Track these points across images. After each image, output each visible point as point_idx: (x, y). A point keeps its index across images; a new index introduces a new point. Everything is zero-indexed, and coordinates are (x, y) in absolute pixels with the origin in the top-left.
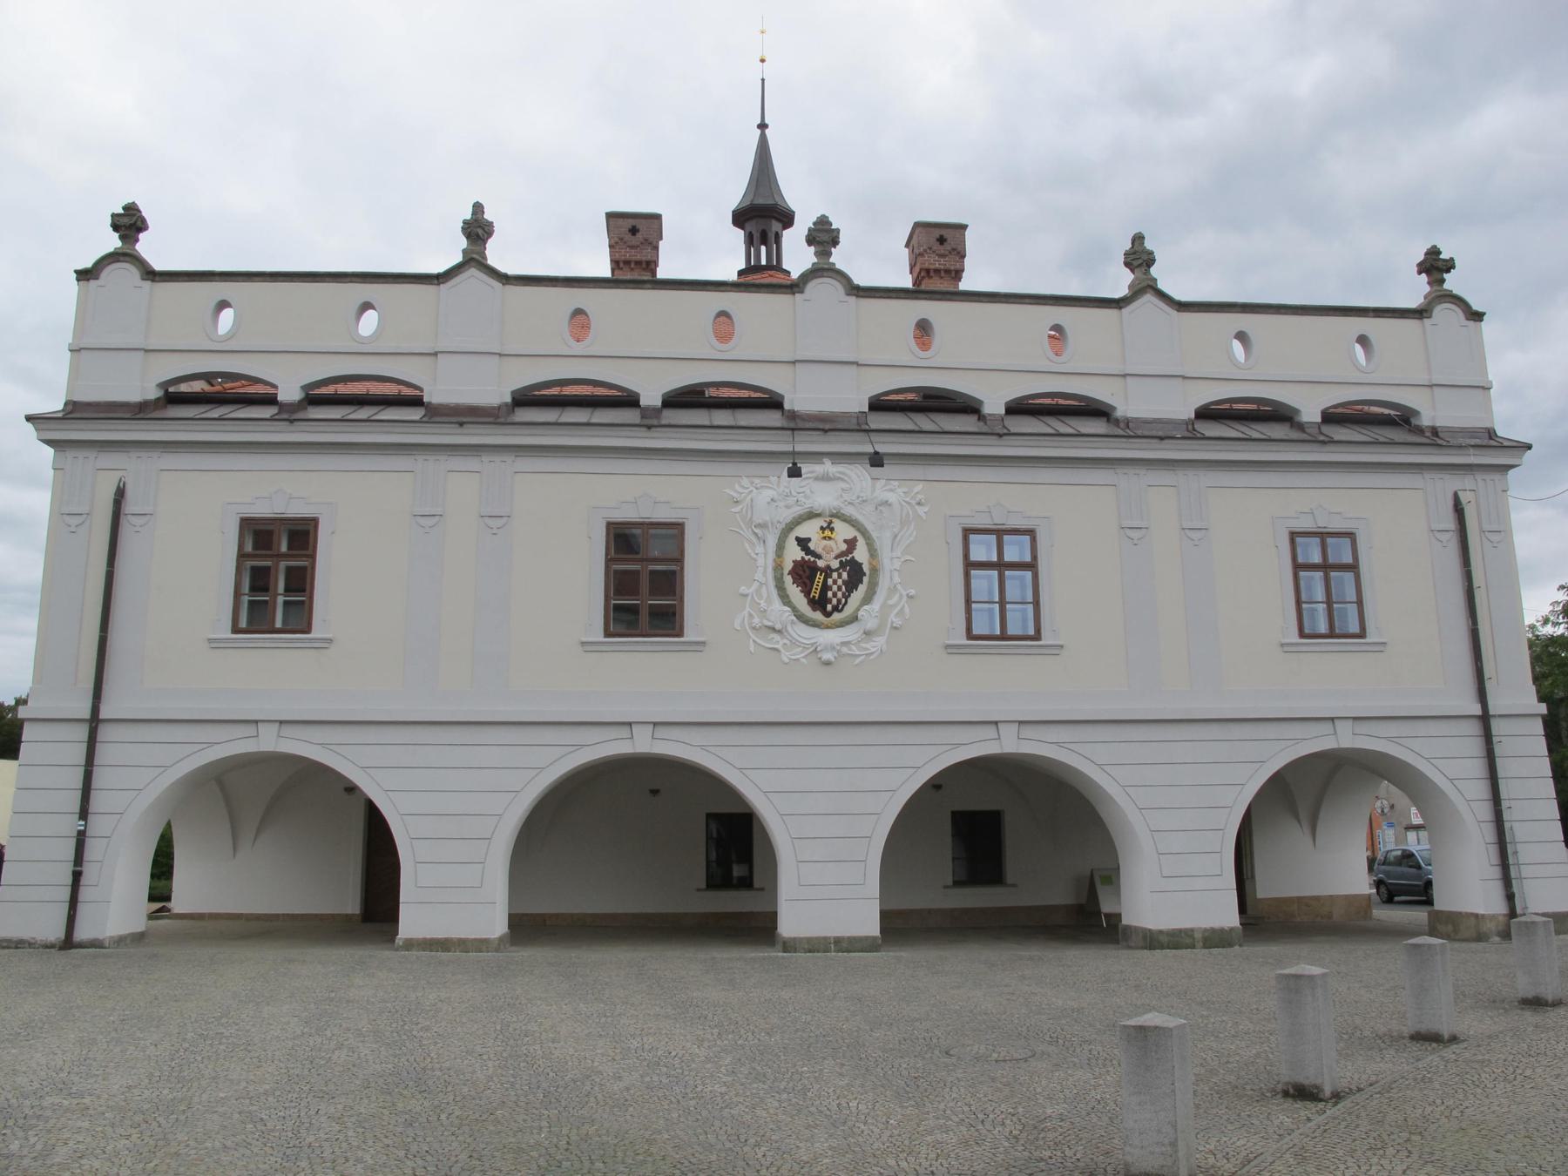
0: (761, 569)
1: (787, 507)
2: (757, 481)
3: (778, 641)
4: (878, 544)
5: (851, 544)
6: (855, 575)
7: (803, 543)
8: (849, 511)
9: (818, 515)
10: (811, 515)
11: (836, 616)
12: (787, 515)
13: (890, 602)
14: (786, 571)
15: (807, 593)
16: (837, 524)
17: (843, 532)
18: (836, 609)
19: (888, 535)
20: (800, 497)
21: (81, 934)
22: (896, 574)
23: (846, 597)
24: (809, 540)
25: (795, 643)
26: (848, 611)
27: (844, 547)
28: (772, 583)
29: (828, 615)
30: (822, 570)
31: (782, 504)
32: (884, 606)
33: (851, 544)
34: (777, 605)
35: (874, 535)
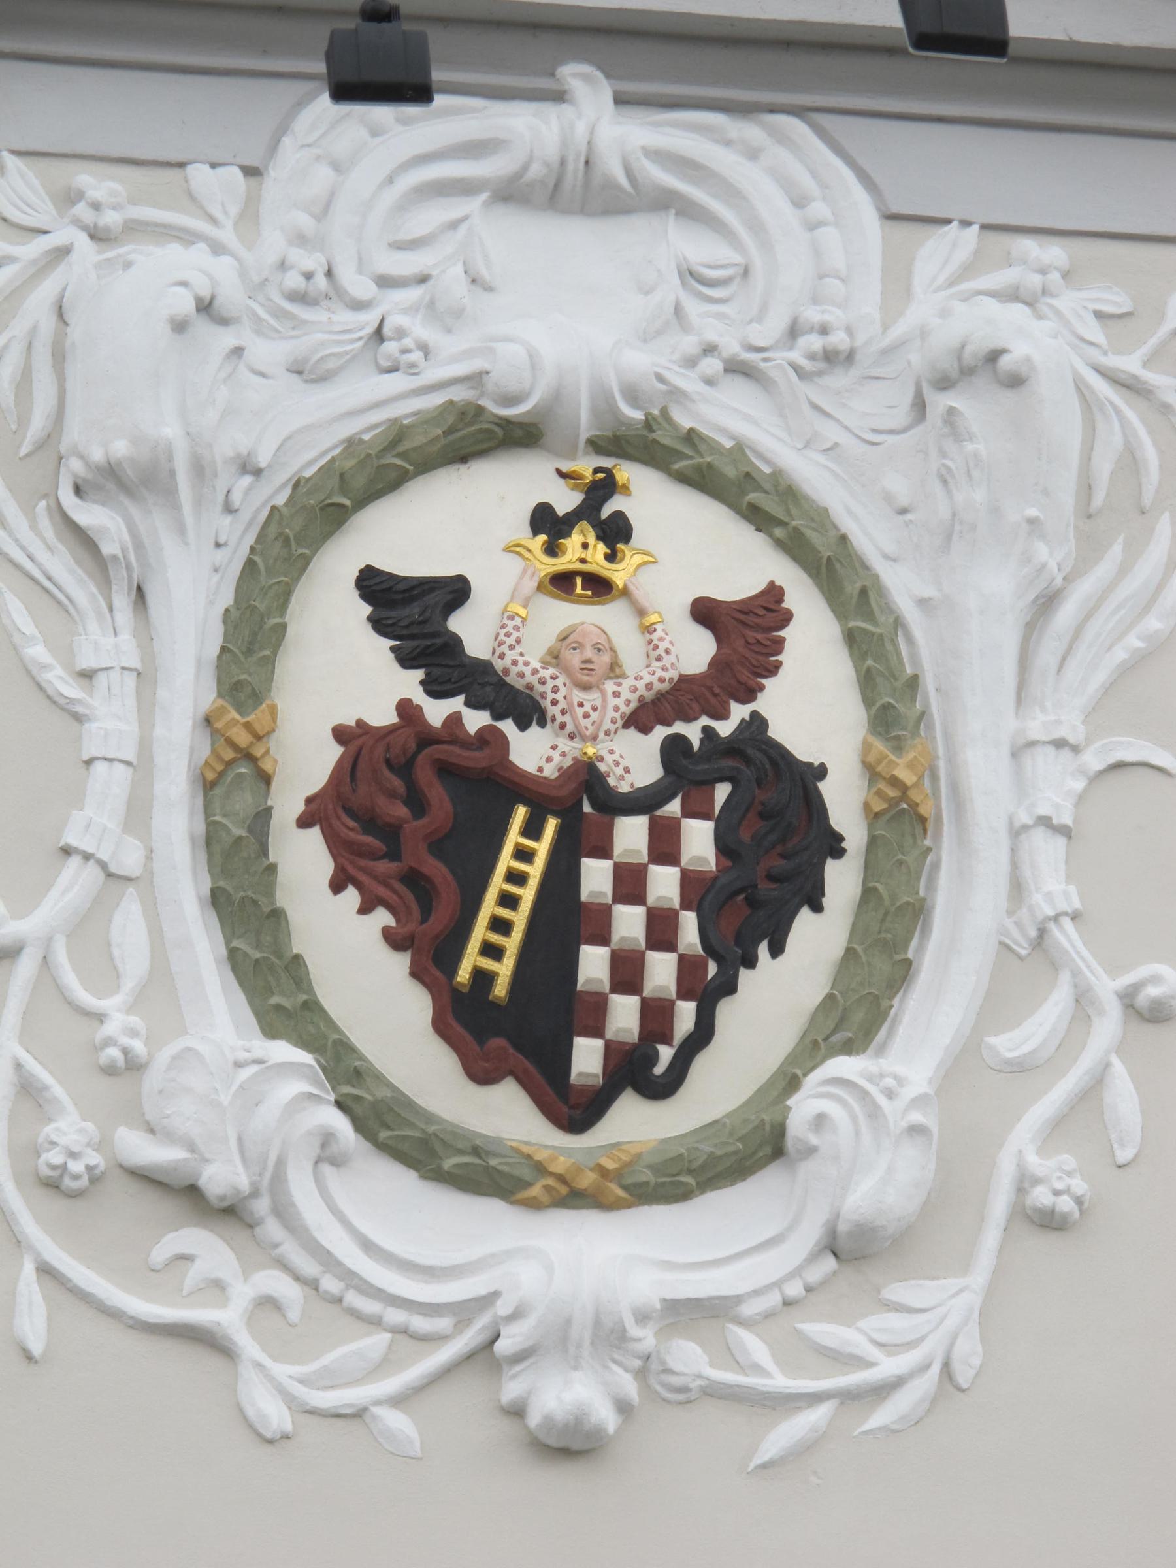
0: (111, 782)
1: (306, 371)
2: (97, 184)
3: (220, 1283)
4: (924, 647)
5: (747, 634)
6: (771, 841)
7: (414, 613)
8: (724, 415)
9: (519, 436)
10: (476, 434)
11: (633, 1123)
12: (311, 427)
13: (1009, 1044)
14: (288, 803)
15: (430, 950)
16: (649, 499)
17: (687, 550)
18: (640, 1072)
19: (993, 589)
20: (395, 308)
21: (130, 755)
22: (1047, 852)
23: (709, 990)
24: (455, 592)
25: (337, 1298)
26: (718, 1087)
27: (695, 651)
28: (185, 884)
29: (577, 1110)
30: (540, 799)
31: (269, 352)
32: (964, 1064)
33: (747, 634)
34: (220, 1018)
35: (902, 585)
